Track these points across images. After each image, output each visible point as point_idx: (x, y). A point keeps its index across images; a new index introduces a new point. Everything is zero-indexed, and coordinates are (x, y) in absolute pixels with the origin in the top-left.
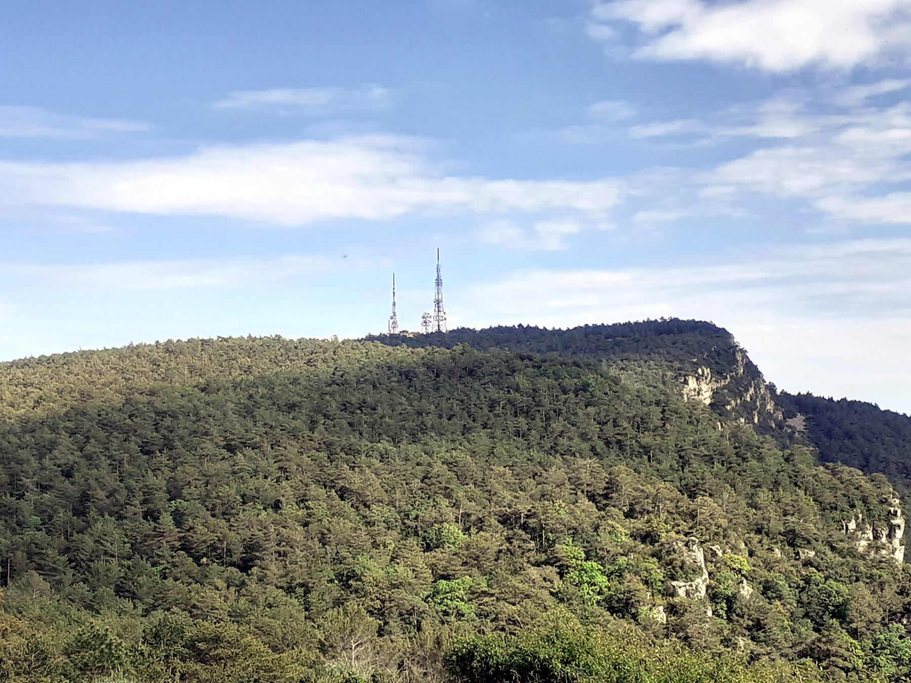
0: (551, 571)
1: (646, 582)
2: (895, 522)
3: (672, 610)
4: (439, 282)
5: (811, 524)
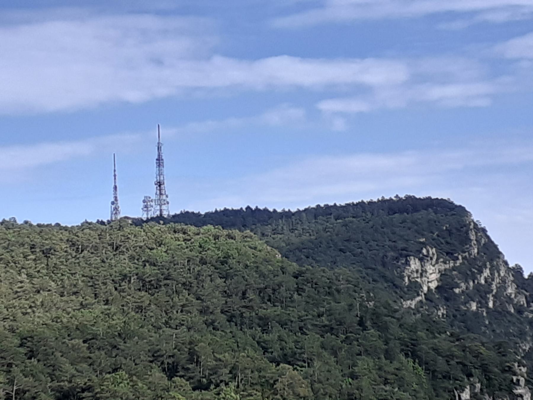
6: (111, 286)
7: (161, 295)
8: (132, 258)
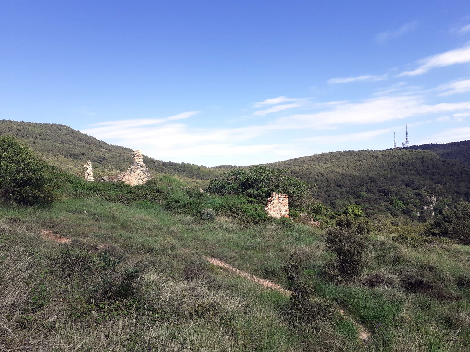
0: (388, 203)
1: (415, 206)
3: (422, 213)
4: (407, 133)
6: (392, 165)
7: (405, 167)
8: (398, 158)
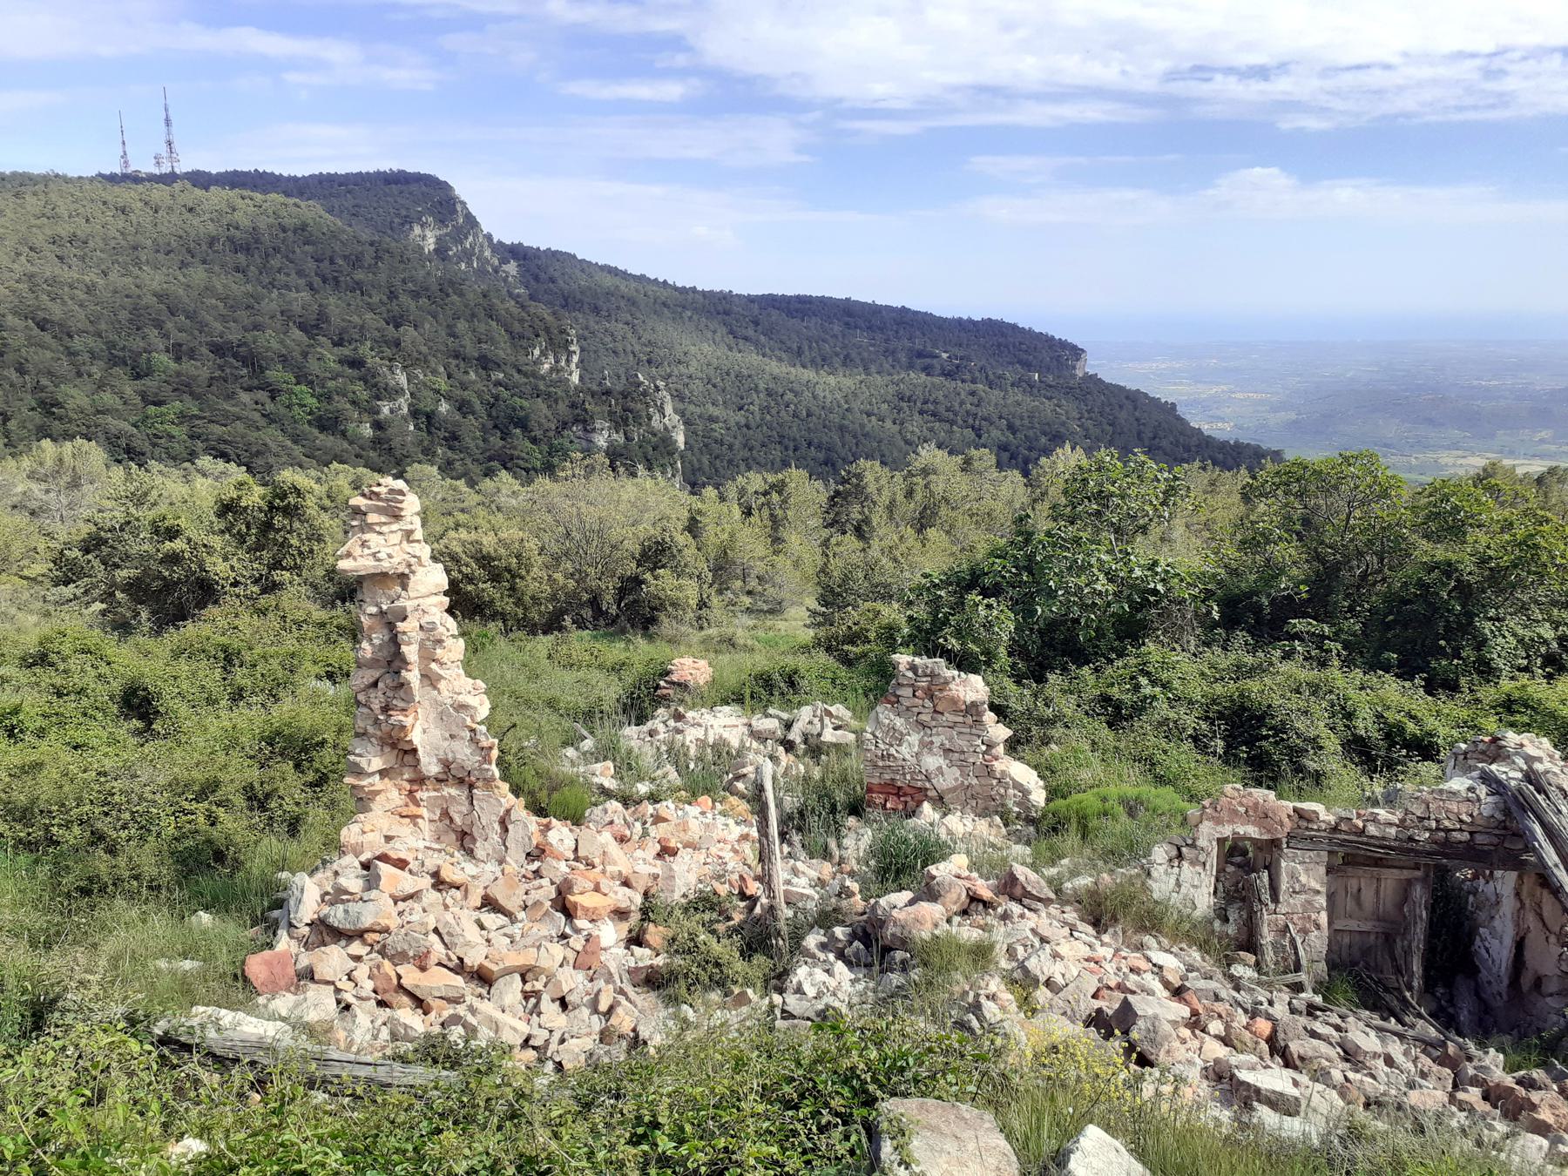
0: (263, 396)
1: (353, 403)
2: (573, 348)
3: (378, 426)
4: (168, 122)
5: (502, 349)
